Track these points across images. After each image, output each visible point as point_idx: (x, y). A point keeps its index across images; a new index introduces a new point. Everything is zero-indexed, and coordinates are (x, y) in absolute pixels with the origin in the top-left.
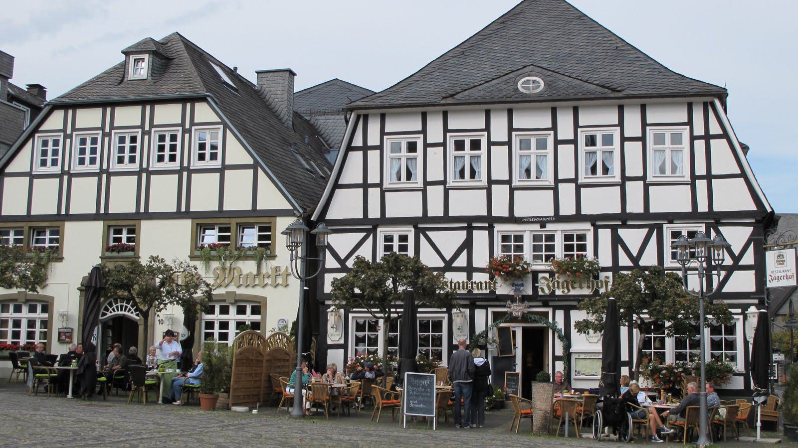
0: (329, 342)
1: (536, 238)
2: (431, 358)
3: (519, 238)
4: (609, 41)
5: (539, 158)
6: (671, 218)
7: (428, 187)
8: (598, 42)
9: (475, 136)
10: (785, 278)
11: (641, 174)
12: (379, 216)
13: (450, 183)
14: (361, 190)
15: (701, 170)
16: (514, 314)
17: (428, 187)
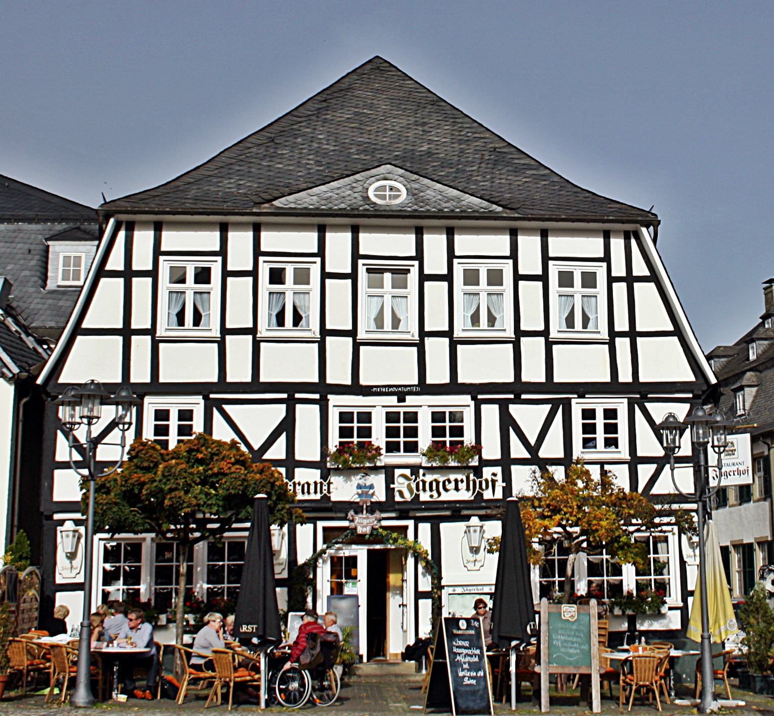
0: (59, 580)
1: (391, 417)
2: (226, 598)
3: (366, 417)
4: (483, 138)
5: (297, 296)
6: (583, 389)
7: (228, 338)
8: (466, 139)
9: (203, 262)
10: (736, 473)
11: (541, 327)
12: (148, 380)
13: (262, 333)
14: (119, 339)
15: (622, 325)
16: (360, 530)
17: (228, 338)
